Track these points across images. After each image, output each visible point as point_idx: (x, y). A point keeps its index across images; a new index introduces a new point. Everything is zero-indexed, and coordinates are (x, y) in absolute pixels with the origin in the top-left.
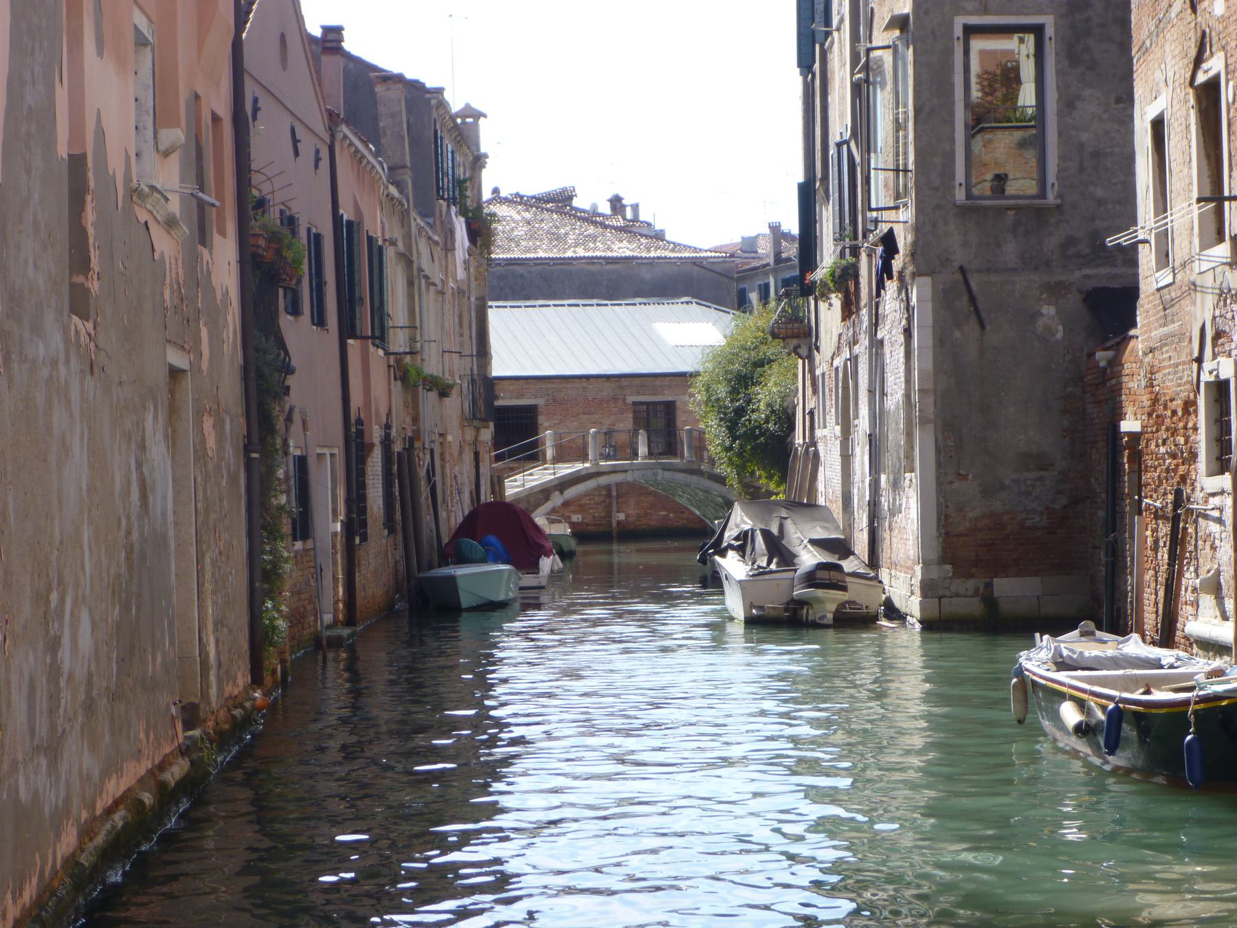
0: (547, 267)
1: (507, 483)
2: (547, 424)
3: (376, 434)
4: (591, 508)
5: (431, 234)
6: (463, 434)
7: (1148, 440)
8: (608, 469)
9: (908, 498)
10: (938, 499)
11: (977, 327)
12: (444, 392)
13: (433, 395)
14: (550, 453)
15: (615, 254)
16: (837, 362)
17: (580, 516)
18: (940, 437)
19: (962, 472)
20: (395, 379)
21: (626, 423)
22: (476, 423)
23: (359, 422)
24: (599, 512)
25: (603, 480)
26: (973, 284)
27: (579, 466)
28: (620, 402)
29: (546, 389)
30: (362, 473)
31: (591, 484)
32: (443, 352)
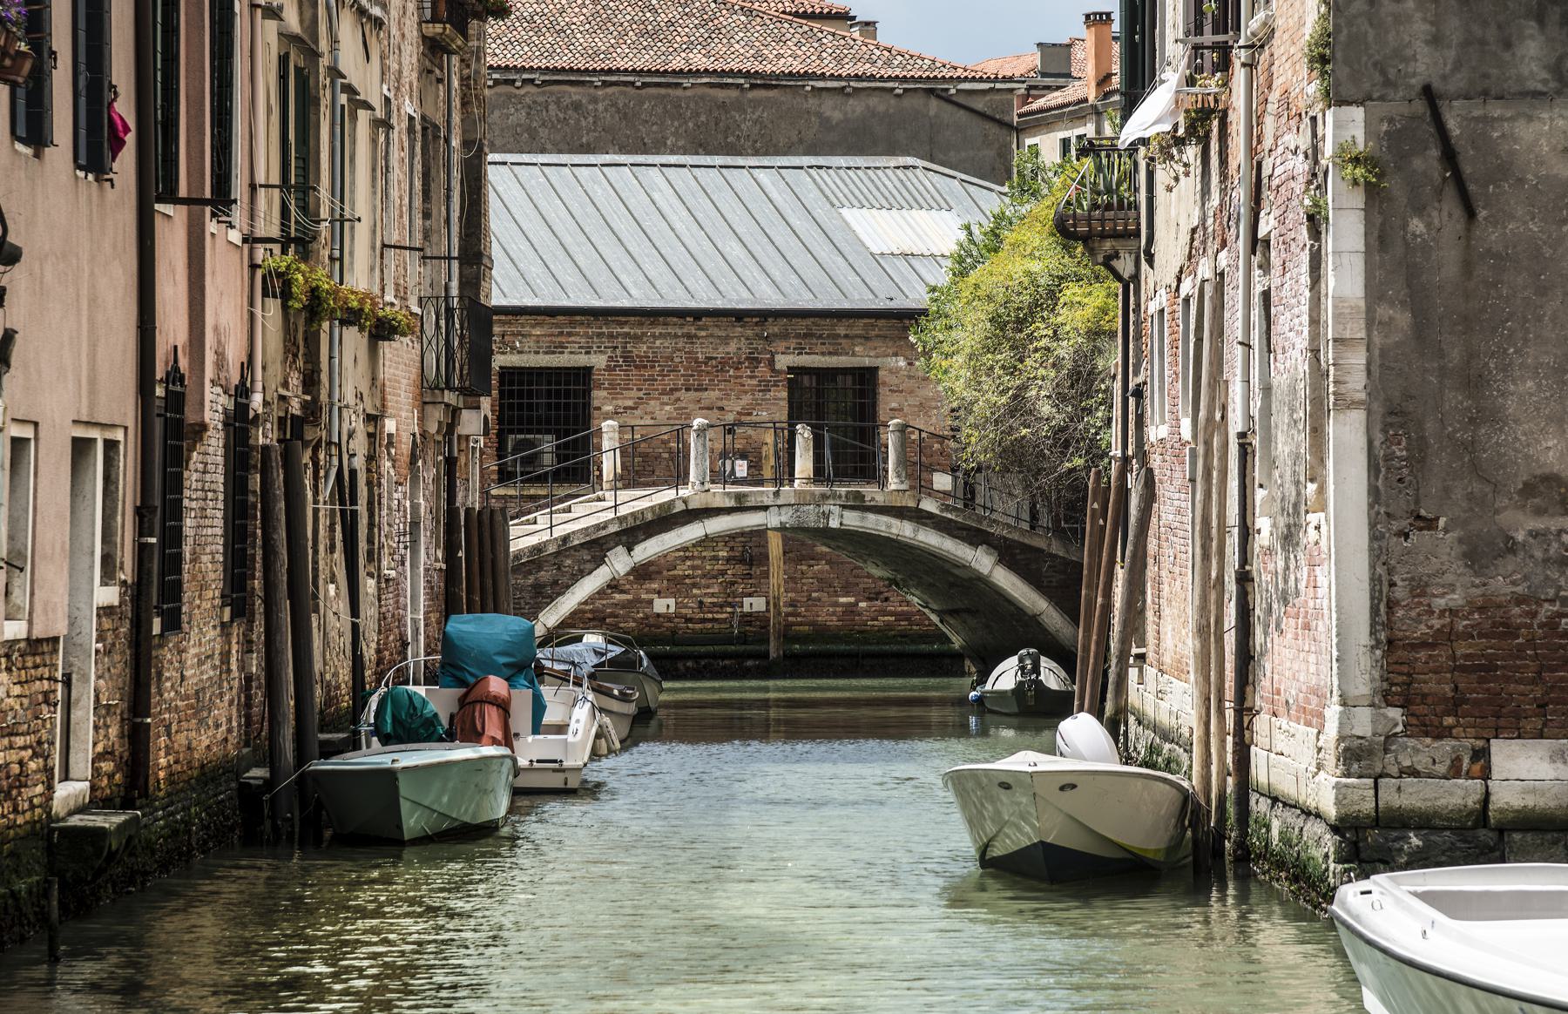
0: (629, 89)
1: (515, 530)
2: (608, 408)
3: (213, 406)
4: (694, 585)
6: (422, 419)
9: (1312, 565)
10: (1372, 567)
11: (1458, 212)
12: (382, 331)
13: (354, 340)
14: (609, 464)
15: (769, 68)
16: (1187, 287)
17: (672, 602)
18: (1379, 438)
19: (1423, 513)
20: (265, 294)
21: (776, 406)
22: (450, 397)
23: (174, 376)
24: (711, 592)
26: (1453, 125)
27: (667, 495)
28: (763, 369)
29: (611, 336)
30: (174, 484)
31: (691, 533)
32: (384, 246)
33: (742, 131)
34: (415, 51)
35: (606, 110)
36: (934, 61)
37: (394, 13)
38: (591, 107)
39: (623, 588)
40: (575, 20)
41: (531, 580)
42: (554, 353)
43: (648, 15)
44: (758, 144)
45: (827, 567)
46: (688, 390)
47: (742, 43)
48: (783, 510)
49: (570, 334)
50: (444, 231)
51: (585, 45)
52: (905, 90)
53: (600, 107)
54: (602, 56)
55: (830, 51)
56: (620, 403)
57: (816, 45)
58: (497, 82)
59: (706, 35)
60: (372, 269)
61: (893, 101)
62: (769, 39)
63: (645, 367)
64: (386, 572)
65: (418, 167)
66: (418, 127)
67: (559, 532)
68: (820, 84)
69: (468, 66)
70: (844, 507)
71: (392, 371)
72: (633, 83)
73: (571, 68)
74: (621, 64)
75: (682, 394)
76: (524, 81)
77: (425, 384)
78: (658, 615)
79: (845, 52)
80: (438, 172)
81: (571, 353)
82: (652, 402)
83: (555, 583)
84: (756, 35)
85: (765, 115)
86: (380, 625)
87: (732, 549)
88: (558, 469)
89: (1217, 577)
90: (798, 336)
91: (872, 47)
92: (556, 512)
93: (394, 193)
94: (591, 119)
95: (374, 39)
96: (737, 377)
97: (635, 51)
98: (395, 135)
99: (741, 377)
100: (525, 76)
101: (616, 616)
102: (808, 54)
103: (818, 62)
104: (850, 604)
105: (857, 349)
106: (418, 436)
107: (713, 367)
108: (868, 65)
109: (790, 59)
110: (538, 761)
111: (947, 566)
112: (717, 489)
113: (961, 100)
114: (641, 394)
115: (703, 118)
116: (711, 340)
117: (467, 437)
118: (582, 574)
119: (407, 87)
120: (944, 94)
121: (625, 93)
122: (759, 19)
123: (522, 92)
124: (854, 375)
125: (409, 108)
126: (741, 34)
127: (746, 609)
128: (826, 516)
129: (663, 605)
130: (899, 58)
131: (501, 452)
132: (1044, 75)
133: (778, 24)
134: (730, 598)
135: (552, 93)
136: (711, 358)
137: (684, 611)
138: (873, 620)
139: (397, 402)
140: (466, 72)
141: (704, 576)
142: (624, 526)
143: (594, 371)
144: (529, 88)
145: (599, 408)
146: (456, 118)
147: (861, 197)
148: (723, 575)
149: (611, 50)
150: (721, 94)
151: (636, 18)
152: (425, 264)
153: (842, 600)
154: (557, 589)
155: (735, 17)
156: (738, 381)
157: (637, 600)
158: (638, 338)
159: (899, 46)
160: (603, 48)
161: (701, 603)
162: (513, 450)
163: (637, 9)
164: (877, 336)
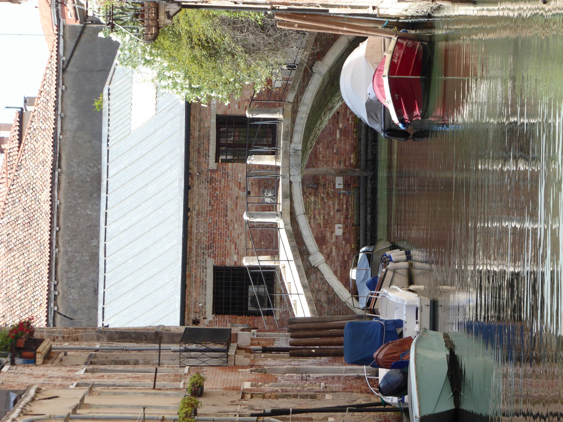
0: (60, 233)
4: (329, 214)
5: (28, 399)
6: (243, 367)
8: (288, 202)
14: (265, 261)
17: (337, 226)
22: (232, 352)
24: (333, 205)
25: (299, 208)
28: (215, 176)
29: (197, 256)
31: (303, 221)
33: (84, 173)
34: (51, 368)
35: (71, 246)
36: (47, 68)
37: (32, 381)
38: (70, 255)
40: (22, 262)
41: (325, 305)
42: (205, 286)
43: (19, 222)
44: (91, 164)
45: (321, 144)
46: (226, 216)
47: (36, 172)
48: (292, 173)
49: (196, 277)
50: (144, 353)
51: (36, 257)
52: (63, 84)
53: (70, 249)
54: (42, 248)
55: (41, 124)
56: (233, 251)
57: (37, 132)
58: (55, 305)
59: (31, 191)
60: (166, 395)
61: (69, 91)
62: (34, 157)
63: (214, 238)
64: (322, 388)
65: (112, 367)
66: (91, 367)
68: (59, 130)
69: (57, 337)
70: (291, 141)
71: (218, 384)
72: (57, 232)
73: (49, 265)
74: (47, 237)
76: (55, 290)
77: (225, 365)
78: (344, 233)
79: (41, 116)
80: (113, 355)
81: (206, 277)
82: (233, 235)
84: (31, 164)
85: (75, 161)
86: (349, 392)
87: (310, 194)
88: (267, 285)
90: (199, 157)
91: (39, 102)
92: (290, 291)
93: (126, 382)
94: (76, 255)
95: (47, 393)
96: (220, 190)
97: (39, 230)
98: (96, 381)
99: (220, 187)
100: (52, 289)
101: (344, 255)
102: (42, 136)
103: (47, 131)
104: (340, 132)
105: (206, 126)
106: (252, 369)
107: (215, 202)
108: (49, 104)
109: (45, 146)
110: (417, 319)
113: (68, 54)
115: (77, 194)
116: (200, 203)
117: (252, 339)
118: (323, 278)
119: (70, 373)
120: (66, 63)
121: (62, 236)
122: (23, 162)
123: (61, 291)
124: (220, 128)
125: (81, 372)
126: (31, 172)
127: (341, 187)
128: (296, 151)
129: (339, 231)
130: (45, 87)
131: (258, 314)
132: (64, 26)
133: (26, 152)
134: (337, 194)
135: (62, 275)
136: (210, 203)
137: (342, 220)
138: (348, 120)
139: (234, 381)
140: (60, 338)
142: (299, 256)
143: (216, 265)
144: (59, 287)
145: (235, 262)
146: (84, 345)
147: (125, 119)
148: (324, 199)
149: (39, 243)
150: (63, 185)
151: (21, 228)
152: (162, 364)
153: (338, 136)
154: (330, 291)
155: (21, 175)
156: (222, 189)
158: (199, 242)
159: (38, 87)
160: (38, 247)
161: (338, 211)
162: (256, 307)
163: (16, 228)
164: (200, 115)
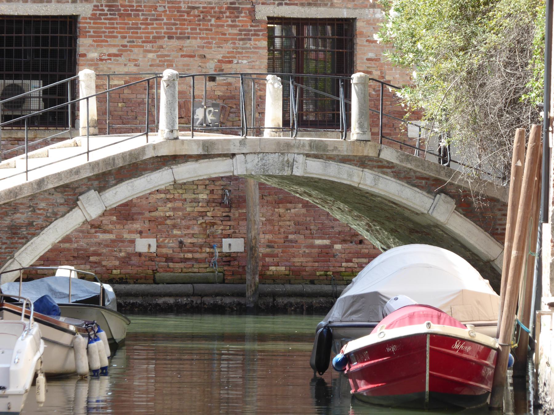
4: (174, 226)
7: (257, 165)
8: (196, 150)
17: (153, 242)
28: (243, 17)
39: (106, 227)
45: (304, 211)
46: (170, 38)
56: (105, 50)
63: (130, 15)
67: (34, 176)
70: (308, 155)
75: (165, 42)
78: (140, 254)
82: (136, 50)
83: (31, 224)
87: (212, 192)
88: (45, 113)
89: (157, 305)
96: (218, 26)
99: (222, 26)
101: (99, 255)
104: (326, 246)
107: (195, 16)
111: (407, 213)
112: (185, 136)
114: (125, 42)
127: (225, 249)
136: (194, 8)
137: (164, 251)
138: (347, 261)
141: (184, 218)
142: (96, 172)
143: (80, 19)
145: (84, 55)
153: (318, 242)
154: (32, 231)
156: (220, 30)
157: (120, 240)
161: (181, 243)
